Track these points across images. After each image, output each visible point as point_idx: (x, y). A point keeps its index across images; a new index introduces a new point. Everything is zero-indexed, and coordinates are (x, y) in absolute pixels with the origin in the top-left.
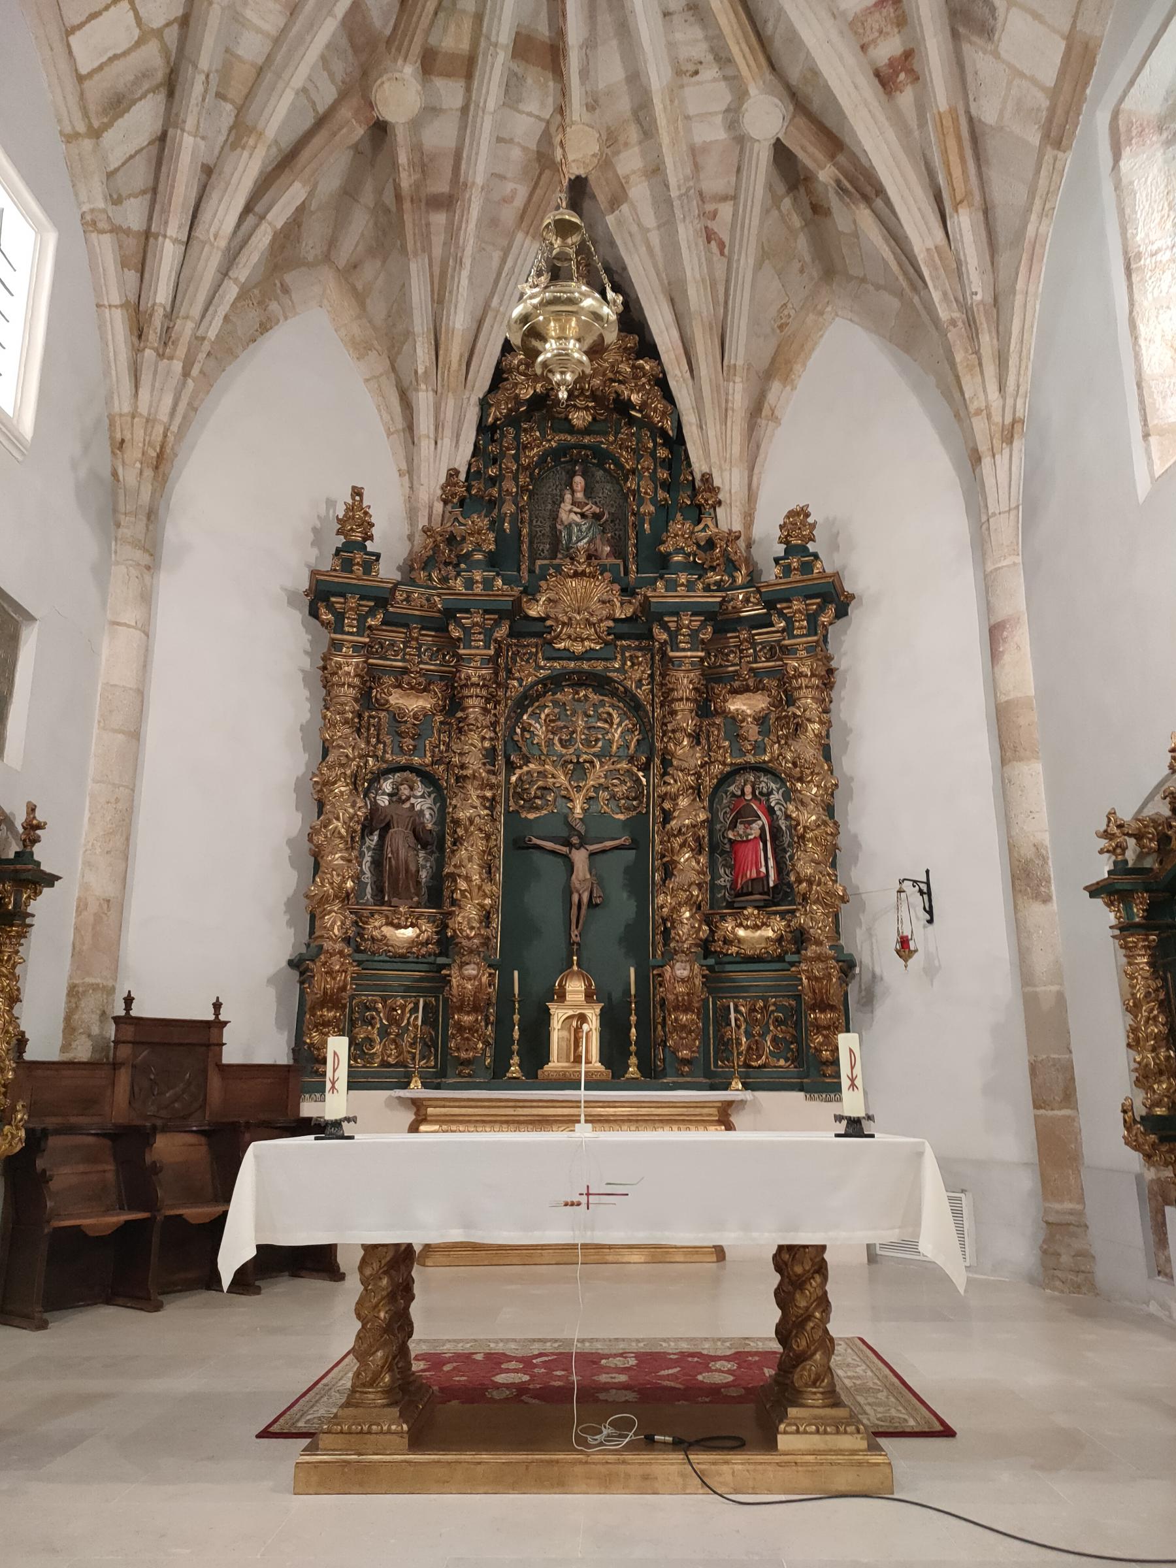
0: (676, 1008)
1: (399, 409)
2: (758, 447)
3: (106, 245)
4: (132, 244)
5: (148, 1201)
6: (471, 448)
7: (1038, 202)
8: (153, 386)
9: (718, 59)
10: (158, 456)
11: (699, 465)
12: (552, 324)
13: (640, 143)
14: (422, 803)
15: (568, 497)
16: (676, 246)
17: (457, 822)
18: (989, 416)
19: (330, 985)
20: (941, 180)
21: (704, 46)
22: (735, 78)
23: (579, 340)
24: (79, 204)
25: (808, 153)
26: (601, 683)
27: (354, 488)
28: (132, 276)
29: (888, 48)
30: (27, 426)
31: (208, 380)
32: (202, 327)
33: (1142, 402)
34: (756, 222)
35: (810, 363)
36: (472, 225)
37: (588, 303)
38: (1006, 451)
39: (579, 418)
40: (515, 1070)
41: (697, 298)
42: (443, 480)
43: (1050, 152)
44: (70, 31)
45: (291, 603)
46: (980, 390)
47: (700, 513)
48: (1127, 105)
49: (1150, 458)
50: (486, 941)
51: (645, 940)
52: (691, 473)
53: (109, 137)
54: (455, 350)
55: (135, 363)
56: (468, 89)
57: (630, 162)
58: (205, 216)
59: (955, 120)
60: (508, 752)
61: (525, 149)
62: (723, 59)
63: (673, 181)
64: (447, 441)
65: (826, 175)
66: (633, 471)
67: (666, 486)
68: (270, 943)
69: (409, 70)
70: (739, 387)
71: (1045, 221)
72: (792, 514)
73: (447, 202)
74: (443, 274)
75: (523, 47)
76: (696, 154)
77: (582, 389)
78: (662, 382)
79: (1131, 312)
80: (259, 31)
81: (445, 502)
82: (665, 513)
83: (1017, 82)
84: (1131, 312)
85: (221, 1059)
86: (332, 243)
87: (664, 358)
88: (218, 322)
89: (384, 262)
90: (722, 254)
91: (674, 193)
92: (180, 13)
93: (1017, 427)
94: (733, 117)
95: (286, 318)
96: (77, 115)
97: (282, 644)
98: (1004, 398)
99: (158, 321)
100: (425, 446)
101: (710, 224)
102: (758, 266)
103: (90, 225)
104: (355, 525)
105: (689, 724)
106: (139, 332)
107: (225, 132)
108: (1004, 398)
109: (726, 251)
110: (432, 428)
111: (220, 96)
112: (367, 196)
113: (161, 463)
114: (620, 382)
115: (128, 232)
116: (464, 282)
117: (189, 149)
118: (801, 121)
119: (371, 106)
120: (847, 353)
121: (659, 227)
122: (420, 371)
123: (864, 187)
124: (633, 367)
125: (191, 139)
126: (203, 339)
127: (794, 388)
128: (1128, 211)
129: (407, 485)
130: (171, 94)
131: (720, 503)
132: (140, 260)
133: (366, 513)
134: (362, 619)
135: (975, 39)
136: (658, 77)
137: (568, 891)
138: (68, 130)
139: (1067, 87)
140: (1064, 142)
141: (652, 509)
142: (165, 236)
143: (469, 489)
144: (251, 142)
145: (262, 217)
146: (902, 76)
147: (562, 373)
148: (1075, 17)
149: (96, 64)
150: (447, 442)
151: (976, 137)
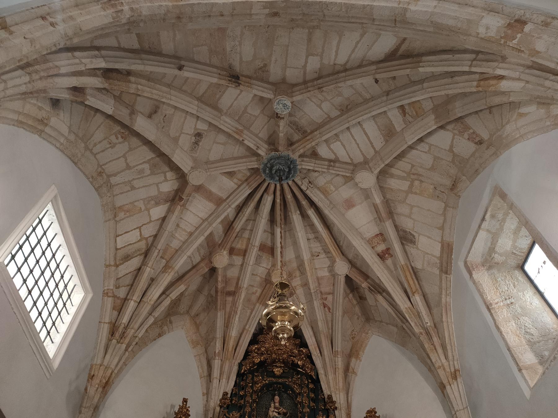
1: (206, 367)
2: (349, 384)
3: (109, 302)
4: (119, 302)
6: (233, 383)
7: (444, 292)
8: (112, 354)
9: (325, 252)
10: (106, 383)
11: (326, 392)
13: (300, 276)
15: (272, 405)
16: (313, 308)
18: (444, 369)
20: (406, 286)
21: (321, 248)
22: (331, 257)
23: (289, 322)
24: (104, 288)
25: (357, 279)
27: (184, 399)
28: (115, 313)
29: (381, 248)
31: (134, 354)
32: (137, 333)
33: (512, 356)
34: (341, 301)
35: (365, 351)
36: (241, 300)
37: (293, 308)
38: (455, 383)
39: (277, 371)
41: (321, 325)
42: (221, 397)
43: (444, 276)
44: (117, 236)
46: (438, 358)
47: (328, 413)
48: (469, 259)
49: (525, 380)
52: (323, 395)
53: (121, 267)
54: (231, 344)
55: (108, 345)
56: (244, 259)
58: (149, 293)
59: (408, 267)
61: (261, 278)
62: (327, 252)
63: (312, 287)
64: (224, 380)
65: (364, 285)
66: (299, 394)
67: (313, 400)
69: (225, 253)
70: (340, 359)
71: (448, 297)
72: (369, 412)
73: (233, 294)
74: (229, 317)
75: (262, 248)
76: (319, 280)
77: (279, 359)
78: (309, 357)
79: (495, 323)
80: (179, 240)
81: (221, 407)
83: (426, 255)
84: (495, 323)
86: (191, 307)
87: (310, 348)
88: (143, 331)
89: (208, 314)
90: (329, 312)
91: (312, 291)
92: (155, 234)
93: (457, 373)
94: (331, 269)
95: (169, 332)
96: (112, 259)
98: (449, 362)
99: (121, 329)
100: (215, 382)
101: (324, 302)
102: (343, 316)
103: (106, 294)
106: (112, 333)
107: (161, 268)
108: (449, 362)
109: (331, 311)
110: (219, 375)
111: (162, 257)
112: (205, 292)
113: (106, 386)
114: (294, 357)
115: (118, 298)
116: (237, 319)
117: (148, 272)
118: (354, 269)
119: (211, 263)
120: (378, 348)
121: (307, 303)
122: (217, 352)
123: (378, 289)
124: (299, 351)
125: (149, 269)
126: (136, 337)
127: (361, 361)
128: (481, 290)
129: (205, 400)
130: (146, 257)
131: (336, 408)
132: (120, 309)
133: (187, 410)
135: (409, 245)
136: (306, 256)
138: (108, 264)
139: (445, 256)
140: (448, 272)
141: (308, 410)
142: (132, 300)
143: (231, 401)
144: (170, 271)
145: (168, 296)
146: (387, 255)
147: (283, 334)
148: (442, 237)
149: (123, 246)
150: (224, 381)
151: (415, 272)
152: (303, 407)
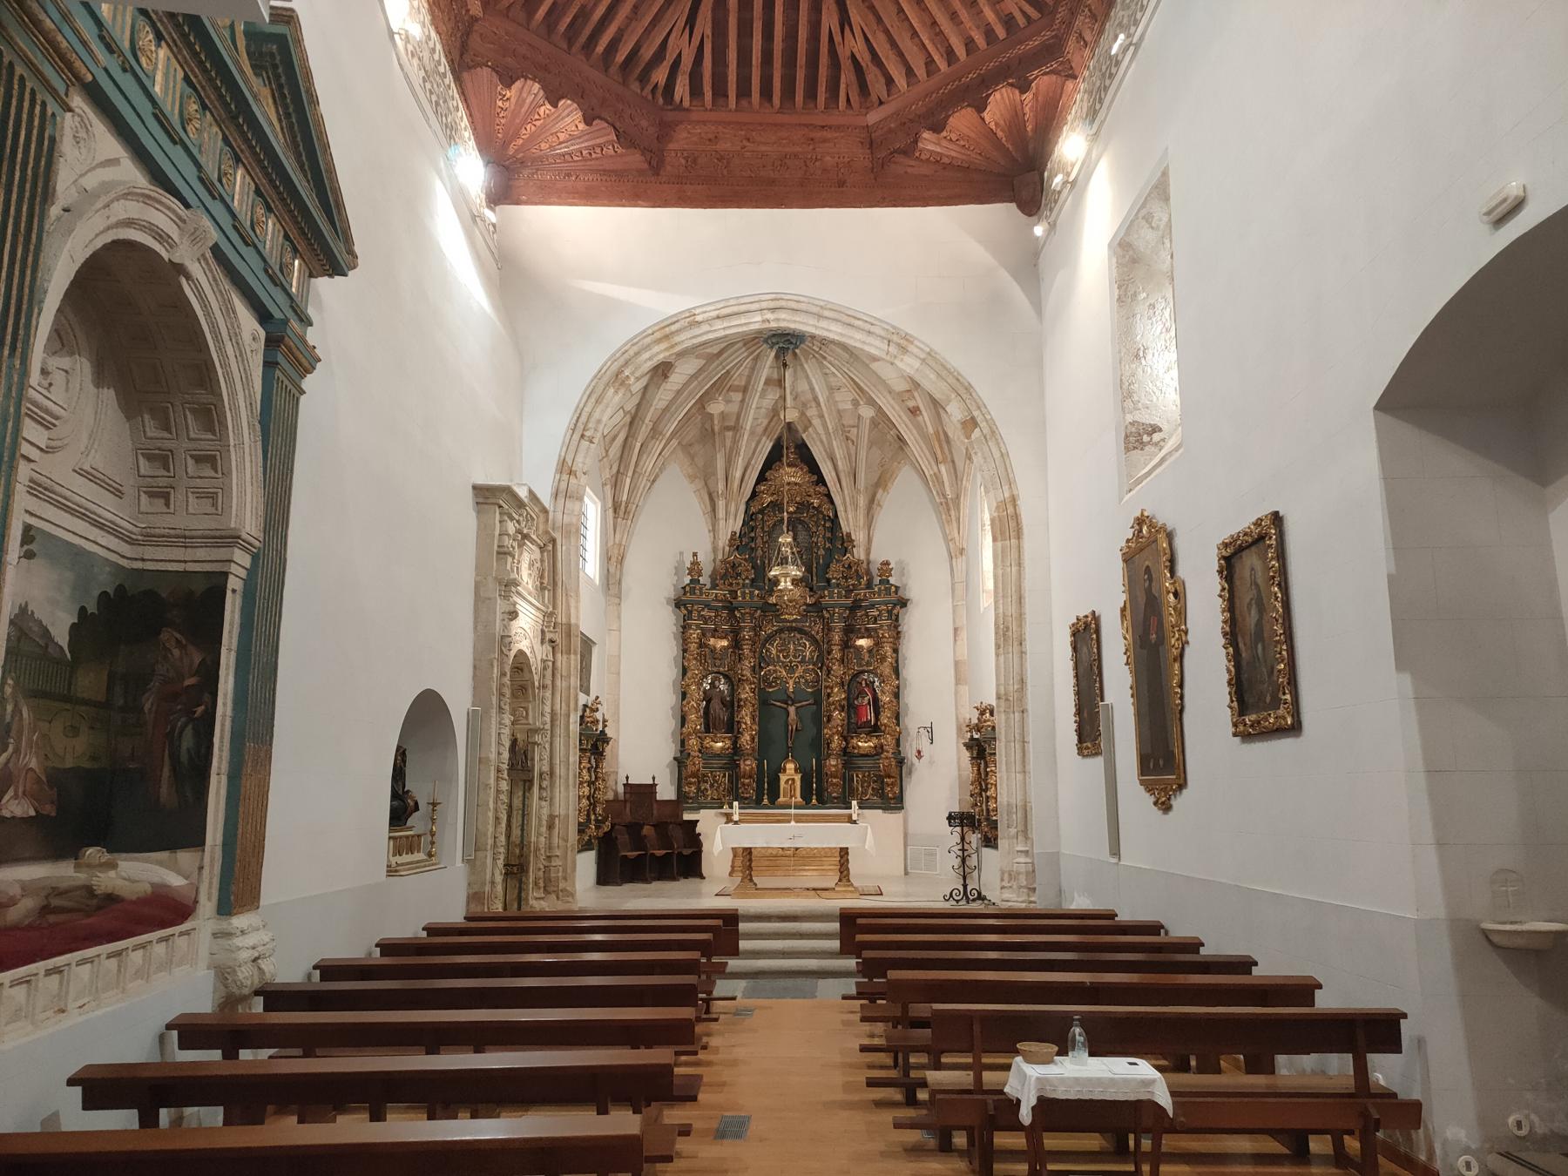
5: (644, 848)
11: (845, 529)
12: (786, 539)
26: (801, 631)
40: (766, 801)
51: (819, 746)
57: (812, 412)
60: (762, 661)
67: (831, 541)
68: (668, 751)
75: (768, 382)
78: (829, 496)
97: (665, 622)
100: (722, 523)
105: (838, 656)
113: (621, 561)
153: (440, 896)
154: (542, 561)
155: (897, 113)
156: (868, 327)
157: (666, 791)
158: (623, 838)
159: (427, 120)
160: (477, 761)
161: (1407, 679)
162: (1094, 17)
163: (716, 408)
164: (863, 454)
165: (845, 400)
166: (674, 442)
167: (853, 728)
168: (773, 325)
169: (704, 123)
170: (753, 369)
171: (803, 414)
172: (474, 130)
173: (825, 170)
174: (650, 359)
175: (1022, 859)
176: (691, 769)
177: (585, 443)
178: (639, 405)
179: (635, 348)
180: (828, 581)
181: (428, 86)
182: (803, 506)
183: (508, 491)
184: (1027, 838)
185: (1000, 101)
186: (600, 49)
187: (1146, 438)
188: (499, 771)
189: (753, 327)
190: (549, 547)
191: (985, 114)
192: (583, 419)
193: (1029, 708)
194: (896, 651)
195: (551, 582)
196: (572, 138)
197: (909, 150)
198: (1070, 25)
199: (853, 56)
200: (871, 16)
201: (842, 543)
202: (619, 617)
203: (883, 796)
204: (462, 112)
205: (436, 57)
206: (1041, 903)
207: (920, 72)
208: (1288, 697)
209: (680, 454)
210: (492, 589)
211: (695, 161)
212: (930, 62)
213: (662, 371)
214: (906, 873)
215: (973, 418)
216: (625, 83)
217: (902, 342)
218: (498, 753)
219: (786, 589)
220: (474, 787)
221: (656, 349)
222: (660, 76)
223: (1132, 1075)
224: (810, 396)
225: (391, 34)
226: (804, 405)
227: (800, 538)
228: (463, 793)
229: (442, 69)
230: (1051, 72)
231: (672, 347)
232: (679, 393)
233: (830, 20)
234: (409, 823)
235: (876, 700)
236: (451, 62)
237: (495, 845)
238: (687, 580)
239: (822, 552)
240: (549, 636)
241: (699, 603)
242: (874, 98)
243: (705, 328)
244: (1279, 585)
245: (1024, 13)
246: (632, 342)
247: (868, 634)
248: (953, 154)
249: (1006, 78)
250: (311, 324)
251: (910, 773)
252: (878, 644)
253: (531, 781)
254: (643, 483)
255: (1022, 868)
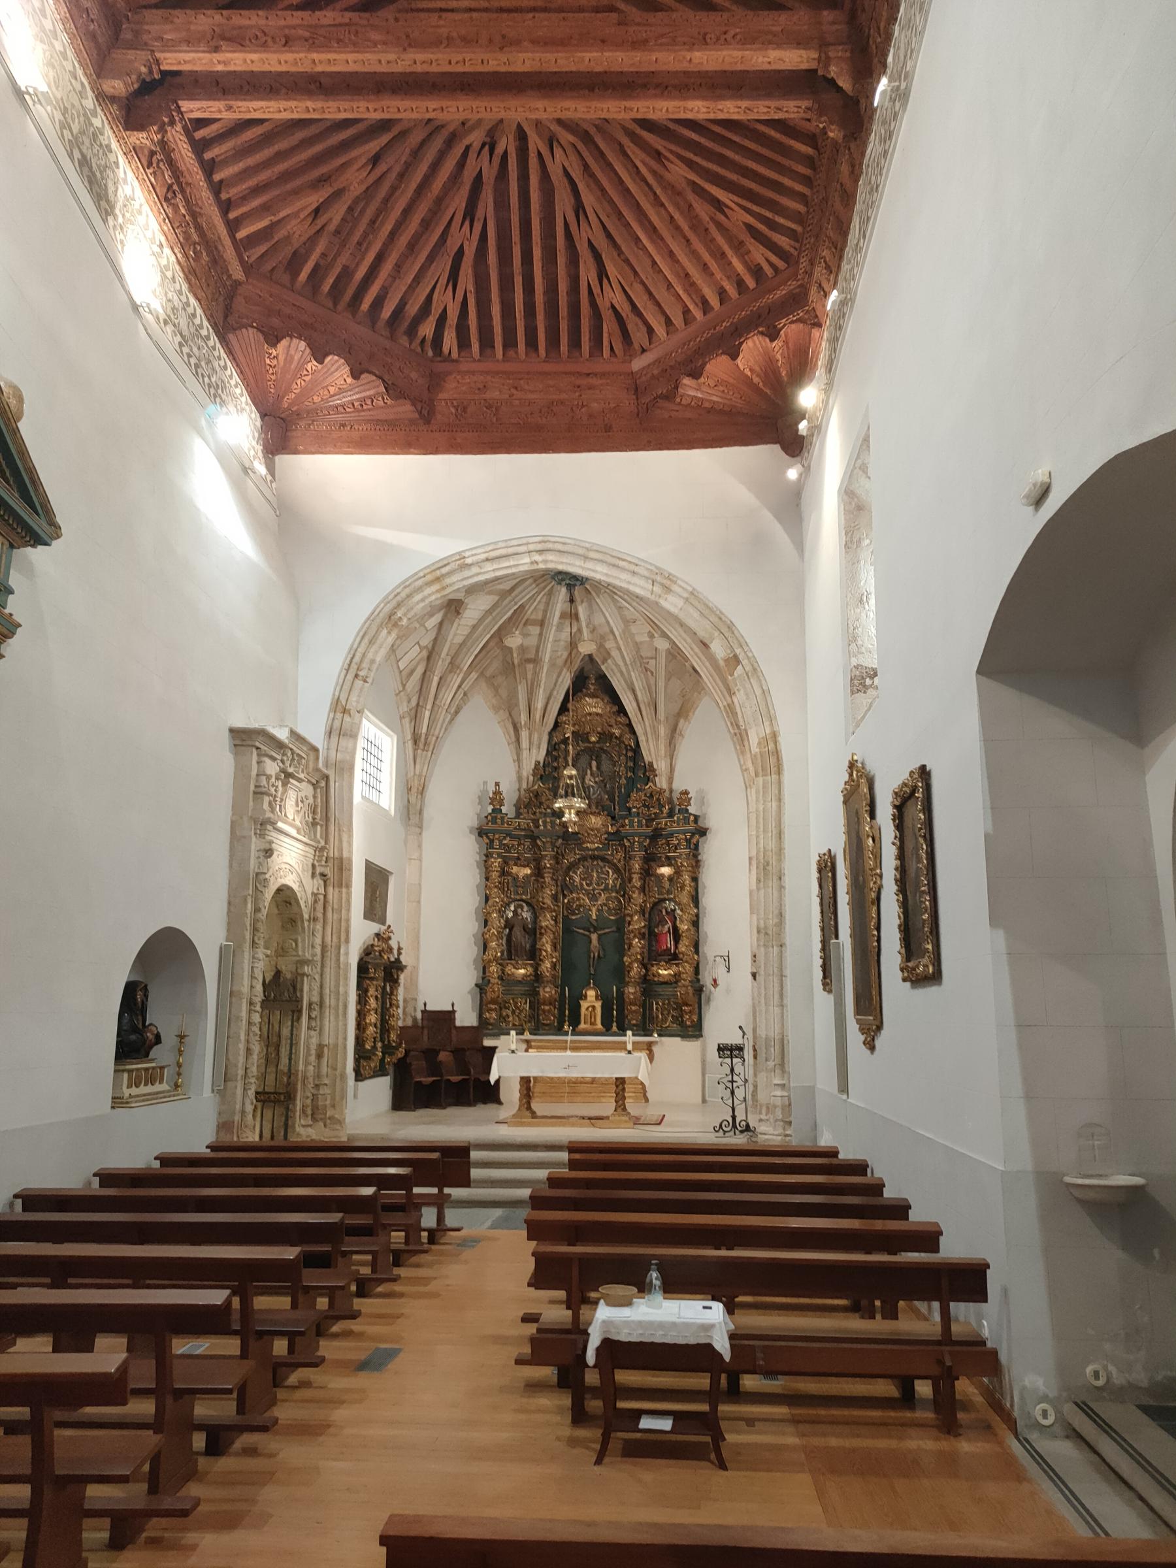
0: (630, 1004)
11: (647, 758)
14: (526, 914)
17: (541, 927)
19: (494, 996)
26: (603, 859)
30: (392, 812)
40: (615, 1028)
45: (471, 832)
50: (554, 976)
51: (620, 973)
54: (538, 715)
57: (610, 645)
60: (565, 888)
67: (633, 770)
72: (381, 1544)
74: (532, 684)
78: (630, 725)
82: (631, 783)
85: (473, 1027)
100: (525, 753)
104: (497, 798)
105: (638, 884)
113: (422, 792)
134: (500, 841)
137: (589, 951)
150: (534, 751)
152: (620, 778)
153: (185, 1122)
154: (315, 797)
155: (658, 361)
156: (632, 567)
157: (466, 1017)
158: (418, 1064)
159: (183, 382)
160: (227, 994)
161: (1000, 934)
162: (828, 267)
163: (514, 641)
164: (661, 684)
165: (640, 632)
166: (474, 675)
167: (653, 955)
168: (542, 566)
169: (473, 373)
170: (547, 604)
171: (601, 646)
172: (247, 387)
173: (591, 416)
174: (423, 600)
175: (779, 1093)
176: (490, 995)
177: (359, 683)
178: (435, 640)
179: (407, 591)
180: (629, 809)
181: (186, 350)
182: (605, 736)
183: (262, 733)
184: (783, 1071)
185: (753, 348)
186: (365, 306)
187: (868, 682)
188: (251, 1003)
189: (521, 569)
190: (321, 783)
191: (739, 361)
192: (357, 659)
193: (788, 943)
194: (695, 879)
195: (325, 817)
196: (341, 391)
197: (671, 395)
198: (811, 275)
199: (613, 307)
200: (627, 268)
201: (641, 771)
202: (420, 846)
203: (682, 1024)
204: (231, 369)
205: (197, 321)
206: (797, 1139)
207: (678, 321)
208: (930, 947)
209: (483, 685)
210: (248, 829)
211: (465, 409)
212: (686, 312)
213: (454, 607)
214: (704, 1101)
215: (735, 656)
216: (392, 337)
217: (666, 582)
218: (250, 986)
219: (571, 820)
220: (226, 1018)
221: (428, 591)
222: (427, 329)
223: (700, 1318)
224: (607, 629)
225: (135, 307)
226: (602, 637)
227: (604, 767)
228: (211, 1027)
229: (204, 332)
230: (799, 320)
231: (444, 588)
232: (474, 627)
233: (587, 273)
234: (152, 1055)
235: (675, 929)
236: (215, 326)
237: (246, 1076)
238: (490, 809)
239: (623, 781)
240: (319, 870)
241: (501, 832)
242: (636, 346)
243: (475, 570)
244: (924, 837)
245: (771, 264)
246: (404, 584)
247: (669, 862)
248: (714, 398)
249: (757, 326)
250: (12, 593)
251: (708, 1000)
252: (678, 873)
253: (300, 1011)
254: (442, 716)
255: (778, 1102)
